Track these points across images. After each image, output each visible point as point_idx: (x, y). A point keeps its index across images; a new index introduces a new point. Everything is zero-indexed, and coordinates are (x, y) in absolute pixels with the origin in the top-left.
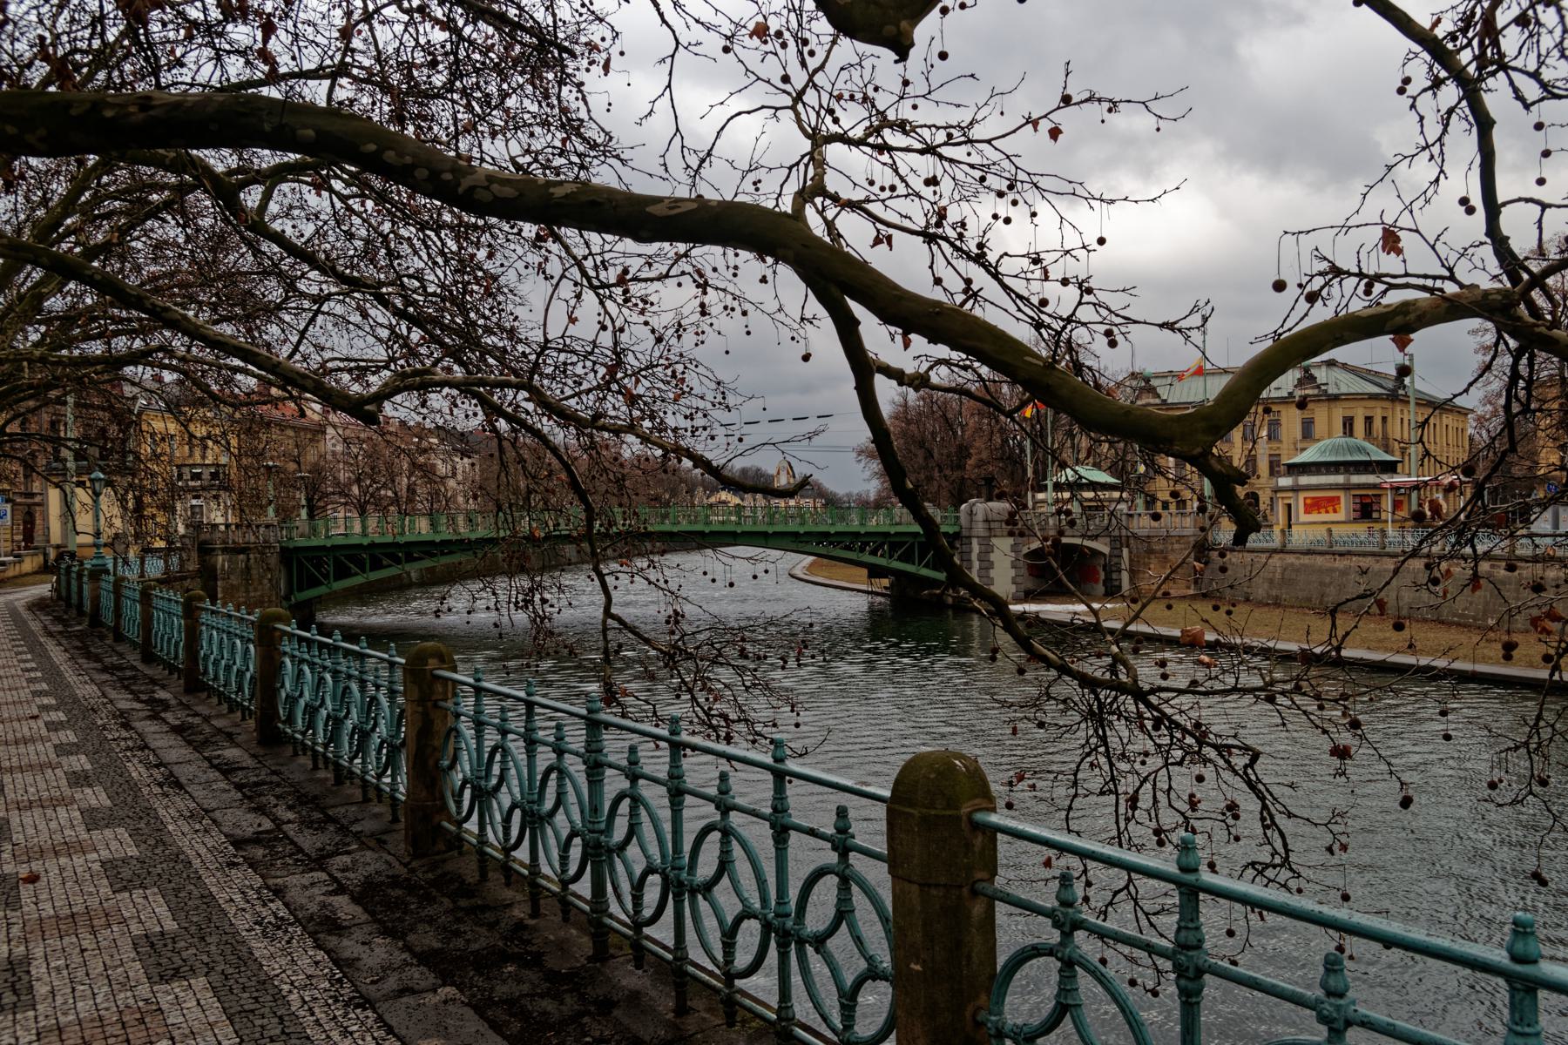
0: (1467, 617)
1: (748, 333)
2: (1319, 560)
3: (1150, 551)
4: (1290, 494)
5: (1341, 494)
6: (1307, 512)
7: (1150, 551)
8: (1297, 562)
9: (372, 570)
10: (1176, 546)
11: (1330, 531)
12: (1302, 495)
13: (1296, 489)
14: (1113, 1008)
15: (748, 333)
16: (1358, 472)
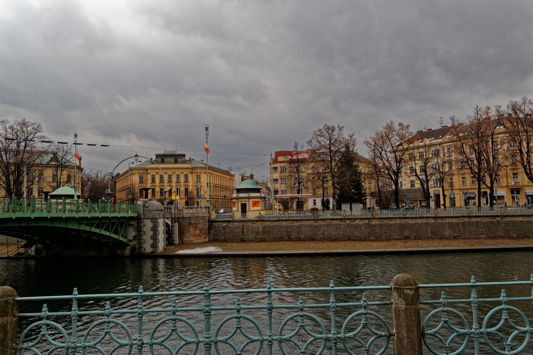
0: (362, 238)
1: (207, 129)
2: (284, 223)
3: (190, 224)
4: (247, 200)
5: (259, 200)
6: (253, 207)
7: (190, 224)
8: (272, 224)
9: (105, 230)
10: (201, 221)
11: (260, 213)
12: (251, 200)
13: (249, 198)
14: (191, 329)
15: (207, 129)
16: (252, 192)
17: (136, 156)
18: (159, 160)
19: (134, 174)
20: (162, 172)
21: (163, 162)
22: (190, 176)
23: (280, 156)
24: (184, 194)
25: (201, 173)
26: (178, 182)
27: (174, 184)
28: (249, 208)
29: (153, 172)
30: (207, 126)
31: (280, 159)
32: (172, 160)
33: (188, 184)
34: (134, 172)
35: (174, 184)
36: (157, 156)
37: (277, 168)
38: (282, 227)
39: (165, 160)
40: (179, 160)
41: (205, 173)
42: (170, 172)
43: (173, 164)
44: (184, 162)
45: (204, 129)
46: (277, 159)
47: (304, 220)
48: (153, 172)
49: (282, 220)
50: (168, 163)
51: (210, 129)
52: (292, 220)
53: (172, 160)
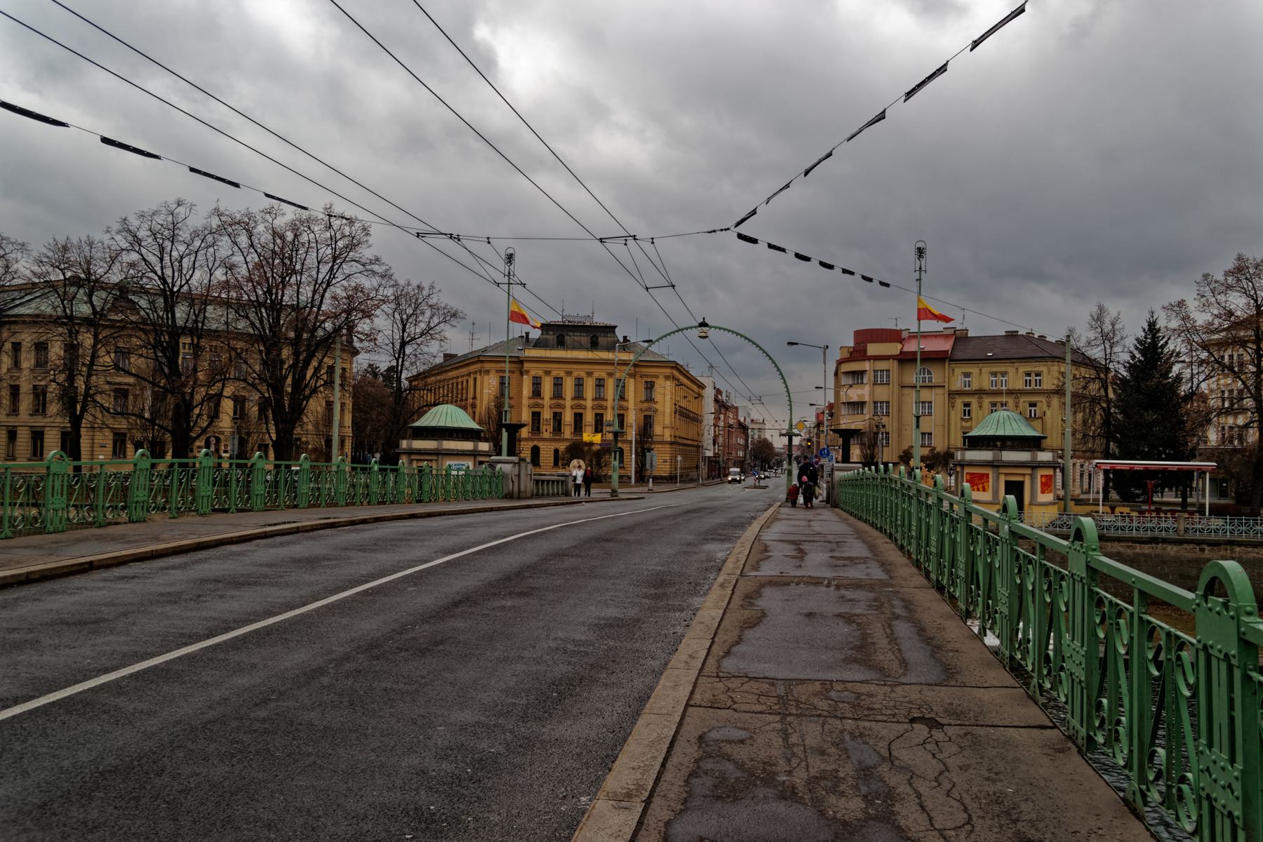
1: (920, 252)
2: (1172, 550)
4: (1028, 471)
8: (1129, 551)
15: (920, 252)
16: (1013, 448)
17: (703, 324)
18: (552, 337)
19: (487, 372)
20: (558, 371)
21: (561, 344)
22: (631, 384)
23: (873, 341)
24: (550, 429)
25: (657, 377)
28: (1033, 495)
29: (536, 370)
30: (921, 245)
31: (873, 349)
32: (585, 339)
34: (487, 366)
35: (568, 402)
36: (545, 327)
37: (862, 373)
38: (1164, 563)
39: (567, 338)
40: (602, 340)
41: (667, 378)
42: (579, 372)
43: (588, 350)
44: (611, 348)
45: (913, 254)
46: (865, 351)
47: (1239, 544)
48: (536, 370)
49: (1164, 541)
50: (574, 348)
51: (929, 253)
52: (1198, 542)
53: (585, 339)
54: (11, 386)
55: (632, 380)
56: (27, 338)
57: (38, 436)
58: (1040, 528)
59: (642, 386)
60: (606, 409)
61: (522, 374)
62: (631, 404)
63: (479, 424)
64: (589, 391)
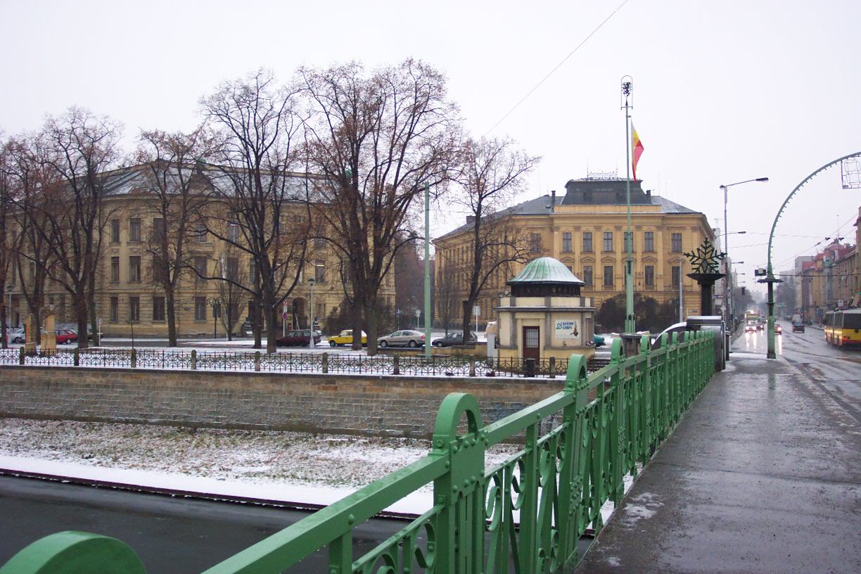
1: (627, 88)
15: (627, 88)
20: (588, 227)
25: (683, 228)
26: (649, 249)
27: (598, 256)
30: (626, 80)
33: (654, 256)
35: (598, 256)
48: (566, 226)
51: (634, 90)
54: (113, 258)
55: (660, 233)
56: (123, 214)
57: (134, 301)
58: (512, 370)
59: (669, 237)
60: (594, 261)
61: (552, 230)
62: (660, 256)
63: (577, 275)
64: (618, 246)
